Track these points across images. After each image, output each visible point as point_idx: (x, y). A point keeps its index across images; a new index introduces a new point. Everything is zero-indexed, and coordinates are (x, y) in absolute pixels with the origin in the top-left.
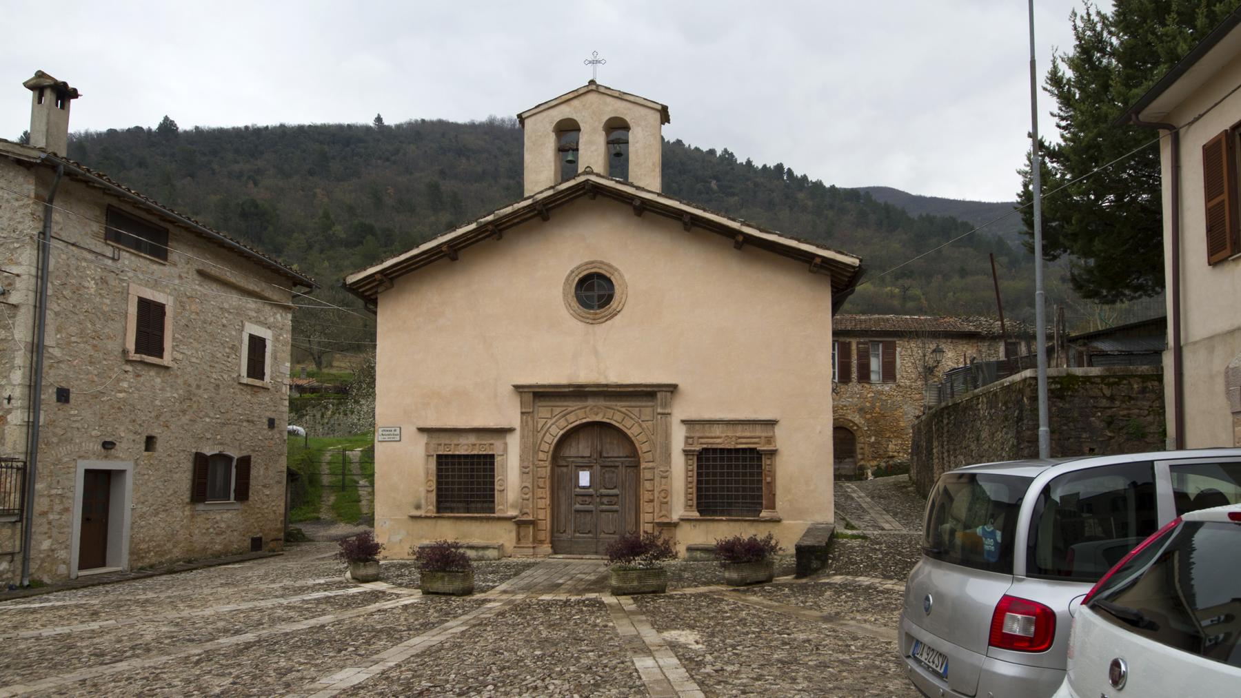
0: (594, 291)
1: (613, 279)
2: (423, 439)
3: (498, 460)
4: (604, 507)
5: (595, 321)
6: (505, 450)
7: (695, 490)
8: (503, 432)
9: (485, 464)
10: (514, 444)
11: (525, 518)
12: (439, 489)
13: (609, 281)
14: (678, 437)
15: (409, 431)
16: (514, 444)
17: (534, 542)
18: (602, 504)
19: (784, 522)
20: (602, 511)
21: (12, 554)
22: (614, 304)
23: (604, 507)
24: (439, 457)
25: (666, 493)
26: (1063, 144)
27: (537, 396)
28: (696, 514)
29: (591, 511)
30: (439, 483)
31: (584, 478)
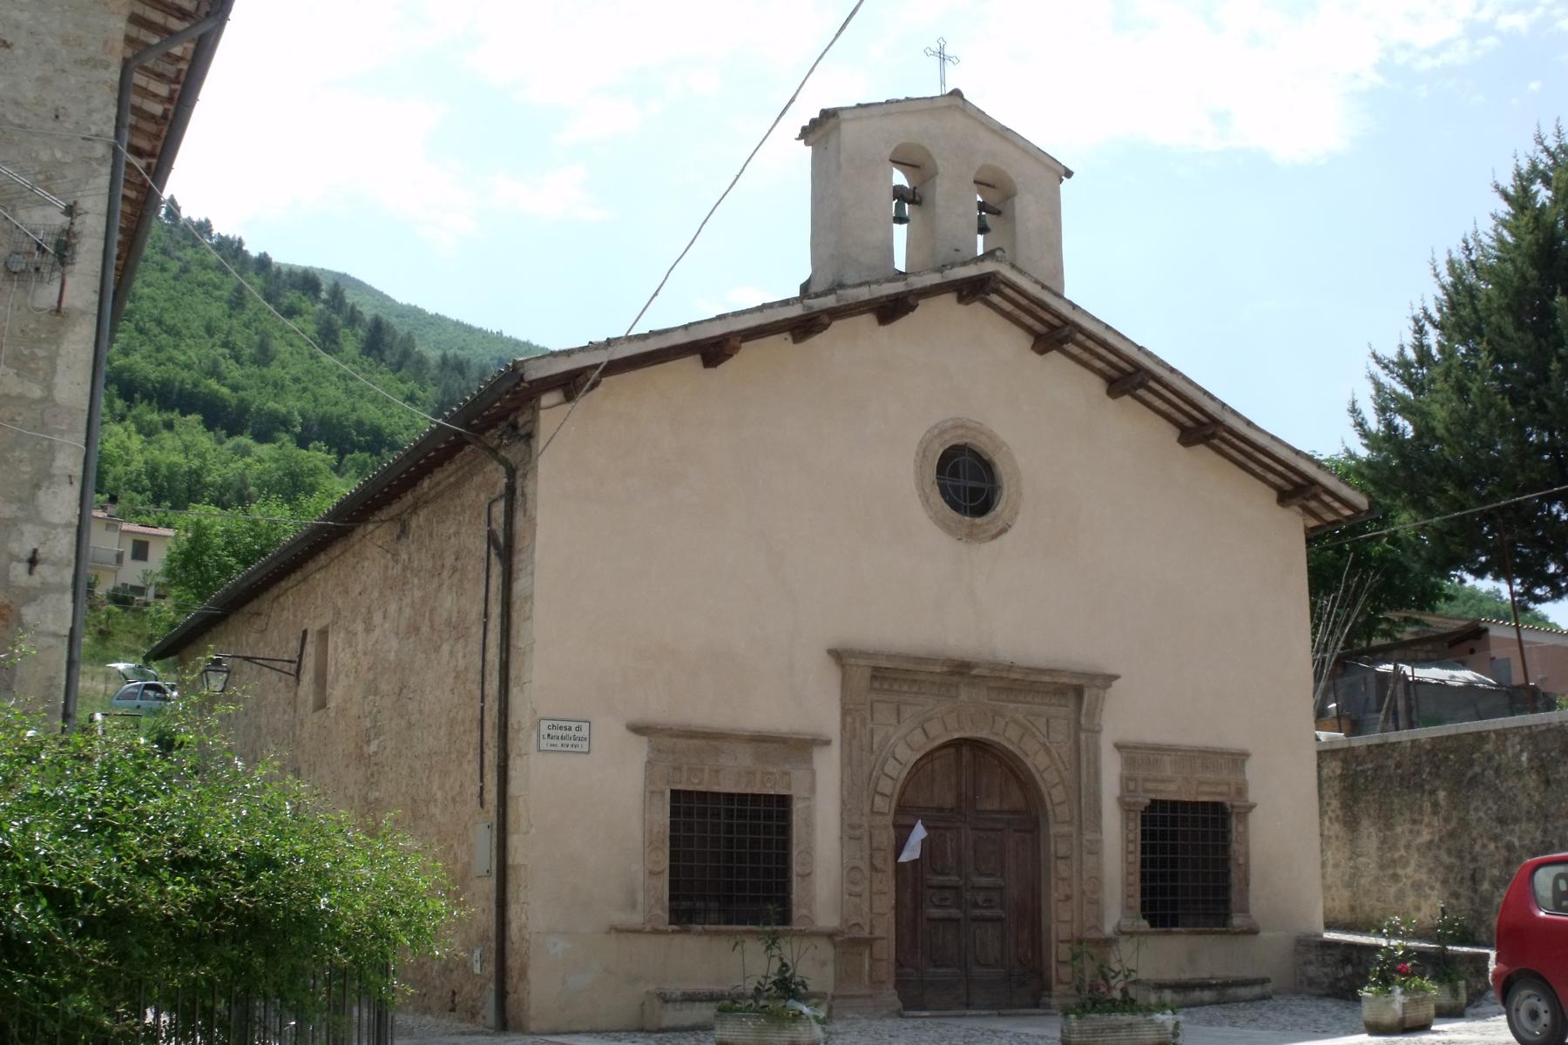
0: (968, 482)
1: (954, 515)
2: (643, 741)
3: (798, 807)
4: (977, 912)
5: (971, 536)
6: (812, 789)
7: (1138, 876)
8: (800, 747)
10: (828, 768)
12: (673, 870)
13: (955, 507)
14: (1111, 772)
15: (609, 732)
18: (975, 905)
19: (1263, 935)
20: (975, 919)
21: (1058, 858)
22: (1000, 508)
23: (977, 912)
25: (1098, 881)
28: (1145, 924)
30: (674, 856)
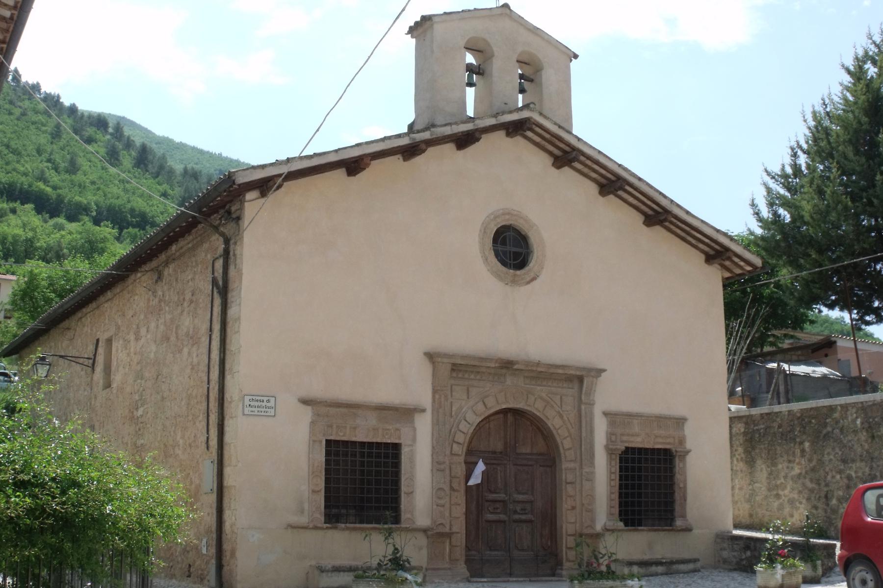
0: (512, 248)
3: (405, 451)
4: (516, 517)
5: (514, 282)
9: (386, 456)
10: (424, 425)
11: (441, 530)
15: (288, 404)
16: (424, 425)
17: (450, 560)
18: (515, 512)
19: (695, 531)
20: (515, 521)
22: (532, 264)
24: (328, 442)
26: (759, 231)
27: (455, 370)
28: (621, 525)
29: (504, 522)
31: (833, 298)
